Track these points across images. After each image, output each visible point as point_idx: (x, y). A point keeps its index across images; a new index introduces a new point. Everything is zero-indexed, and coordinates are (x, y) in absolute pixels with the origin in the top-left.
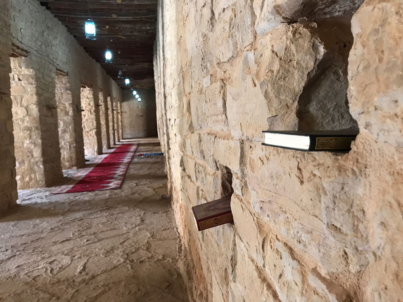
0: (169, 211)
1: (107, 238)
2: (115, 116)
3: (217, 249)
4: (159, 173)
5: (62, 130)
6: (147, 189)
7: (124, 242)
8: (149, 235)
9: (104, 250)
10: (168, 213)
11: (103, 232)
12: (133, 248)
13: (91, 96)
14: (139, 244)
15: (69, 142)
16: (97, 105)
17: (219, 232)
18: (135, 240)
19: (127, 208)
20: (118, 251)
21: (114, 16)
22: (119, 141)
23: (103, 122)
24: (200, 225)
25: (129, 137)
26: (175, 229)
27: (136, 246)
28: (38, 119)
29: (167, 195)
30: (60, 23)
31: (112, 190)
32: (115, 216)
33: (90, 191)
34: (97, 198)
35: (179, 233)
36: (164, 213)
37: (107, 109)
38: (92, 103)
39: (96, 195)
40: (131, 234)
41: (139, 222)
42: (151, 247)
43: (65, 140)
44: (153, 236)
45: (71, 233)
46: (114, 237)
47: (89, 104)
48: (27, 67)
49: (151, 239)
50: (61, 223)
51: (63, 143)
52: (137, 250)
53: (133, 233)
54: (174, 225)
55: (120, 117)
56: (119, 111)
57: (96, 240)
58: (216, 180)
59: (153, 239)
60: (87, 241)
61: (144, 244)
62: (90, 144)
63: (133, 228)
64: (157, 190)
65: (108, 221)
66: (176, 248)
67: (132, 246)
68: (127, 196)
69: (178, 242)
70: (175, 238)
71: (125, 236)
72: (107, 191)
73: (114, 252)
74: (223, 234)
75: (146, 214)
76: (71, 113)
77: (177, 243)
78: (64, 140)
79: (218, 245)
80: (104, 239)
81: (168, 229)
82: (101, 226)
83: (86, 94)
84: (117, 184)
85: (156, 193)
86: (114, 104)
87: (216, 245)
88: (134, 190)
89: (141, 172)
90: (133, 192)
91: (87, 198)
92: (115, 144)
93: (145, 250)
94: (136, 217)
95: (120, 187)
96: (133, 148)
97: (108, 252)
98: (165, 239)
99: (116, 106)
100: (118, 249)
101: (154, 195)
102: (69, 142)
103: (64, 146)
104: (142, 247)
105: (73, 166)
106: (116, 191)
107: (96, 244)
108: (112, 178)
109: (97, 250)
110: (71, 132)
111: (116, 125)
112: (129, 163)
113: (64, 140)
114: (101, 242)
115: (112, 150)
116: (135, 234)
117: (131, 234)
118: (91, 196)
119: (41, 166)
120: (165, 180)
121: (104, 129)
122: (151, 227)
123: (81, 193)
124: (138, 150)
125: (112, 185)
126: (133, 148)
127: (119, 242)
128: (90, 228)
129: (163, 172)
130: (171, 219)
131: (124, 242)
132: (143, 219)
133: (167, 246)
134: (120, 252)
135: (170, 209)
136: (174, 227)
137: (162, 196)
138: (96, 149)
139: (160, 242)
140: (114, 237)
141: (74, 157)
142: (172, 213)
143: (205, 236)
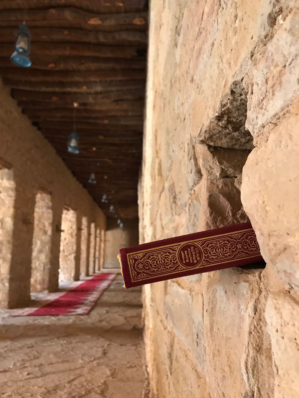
0: (139, 344)
1: (54, 373)
2: (98, 244)
3: (195, 386)
4: (135, 301)
5: (38, 250)
6: (118, 317)
7: (73, 380)
8: (108, 373)
9: (45, 388)
10: (138, 346)
11: (52, 364)
12: (83, 389)
13: (74, 220)
14: (93, 384)
15: (43, 263)
16: (79, 229)
17: (200, 335)
18: (89, 379)
19: (89, 337)
20: (62, 393)
21: (101, 137)
22: (99, 270)
23: (83, 247)
24: (130, 262)
25: (110, 266)
26: (144, 367)
27: (87, 387)
28: (11, 233)
29: (140, 326)
30: (50, 144)
31: (78, 316)
32: (73, 345)
33: (53, 315)
34: (59, 323)
35: (148, 374)
36: (133, 345)
37: (89, 234)
38: (74, 227)
39: (59, 320)
40: (86, 370)
41: (99, 354)
42: (107, 389)
43: (39, 260)
44: (113, 375)
45: (13, 363)
46: (63, 371)
47: (71, 228)
48: (9, 179)
49: (111, 378)
50: (6, 349)
51: (37, 264)
52: (88, 392)
53: (89, 368)
54: (143, 362)
55: (102, 245)
56: (103, 239)
57: (39, 375)
58: (194, 205)
59: (113, 378)
60: (28, 374)
61: (100, 384)
62: (67, 269)
63: (91, 361)
64: (129, 319)
65: (63, 351)
66: (142, 394)
67: (83, 386)
68: (93, 323)
69: (145, 386)
70: (142, 379)
71: (78, 372)
72: (72, 317)
73: (57, 393)
74: (212, 329)
75: (110, 346)
76: (50, 232)
77: (144, 388)
78: (39, 260)
79: (199, 377)
80: (50, 373)
81: (135, 366)
82: (51, 356)
83: (68, 219)
84: (85, 310)
85: (128, 322)
86: (98, 231)
87: (192, 376)
88: (103, 318)
89: (115, 300)
90: (101, 319)
91: (47, 323)
92: (94, 272)
93: (99, 394)
94: (98, 348)
95: (88, 313)
96: (112, 277)
97: (49, 392)
98: (128, 379)
99: (100, 234)
100: (62, 390)
101: (124, 324)
102: (43, 263)
103: (38, 267)
104: (96, 389)
105: (44, 289)
106: (82, 317)
107: (37, 379)
108: (82, 304)
109: (36, 387)
110: (48, 252)
111: (97, 253)
112: (105, 290)
113: (39, 260)
114: (44, 378)
115: (90, 278)
116: (91, 370)
117: (86, 370)
118: (53, 320)
119: (7, 285)
120: (140, 310)
121: (83, 256)
122: (114, 362)
123: (43, 317)
124: (116, 279)
125: (80, 311)
126: (112, 277)
127: (67, 380)
128: (38, 358)
129: (139, 301)
130: (141, 355)
131: (73, 380)
132: (106, 351)
133: (129, 391)
134: (65, 393)
135: (142, 342)
136: (143, 365)
137: (134, 326)
138: (73, 274)
139: (121, 384)
140: (63, 371)
141: (47, 279)
142: (143, 346)
143: (174, 363)
